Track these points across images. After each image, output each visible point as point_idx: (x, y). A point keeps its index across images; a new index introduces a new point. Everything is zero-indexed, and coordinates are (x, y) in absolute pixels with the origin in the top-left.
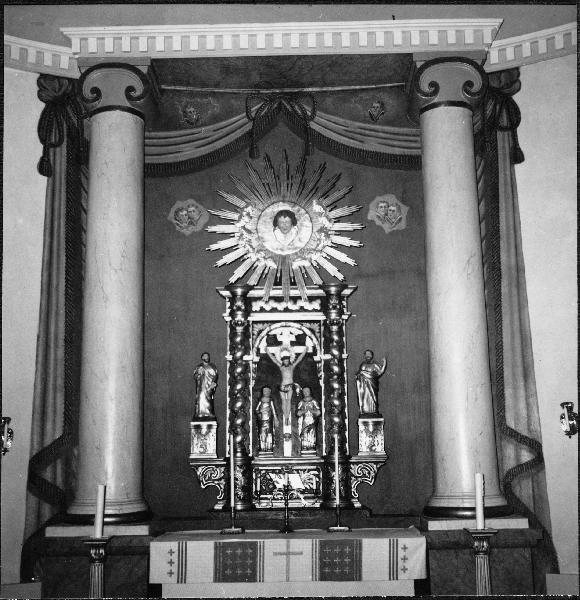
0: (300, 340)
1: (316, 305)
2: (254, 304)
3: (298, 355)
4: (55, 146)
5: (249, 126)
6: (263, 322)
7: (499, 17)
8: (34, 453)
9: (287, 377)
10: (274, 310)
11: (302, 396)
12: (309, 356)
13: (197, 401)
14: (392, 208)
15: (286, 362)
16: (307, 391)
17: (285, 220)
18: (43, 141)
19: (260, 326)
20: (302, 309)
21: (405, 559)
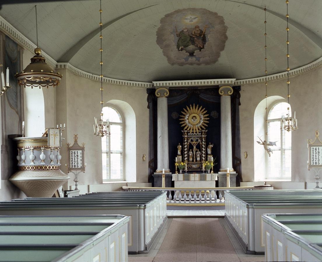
0: (197, 140)
1: (200, 134)
2: (188, 134)
3: (197, 143)
4: (150, 103)
5: (187, 96)
6: (190, 137)
7: (99, 32)
8: (151, 159)
9: (195, 147)
10: (192, 135)
11: (197, 151)
12: (199, 144)
13: (177, 152)
14: (216, 113)
15: (194, 145)
16: (198, 150)
17: (194, 118)
18: (148, 102)
19: (190, 138)
20: (198, 135)
21: (213, 179)
